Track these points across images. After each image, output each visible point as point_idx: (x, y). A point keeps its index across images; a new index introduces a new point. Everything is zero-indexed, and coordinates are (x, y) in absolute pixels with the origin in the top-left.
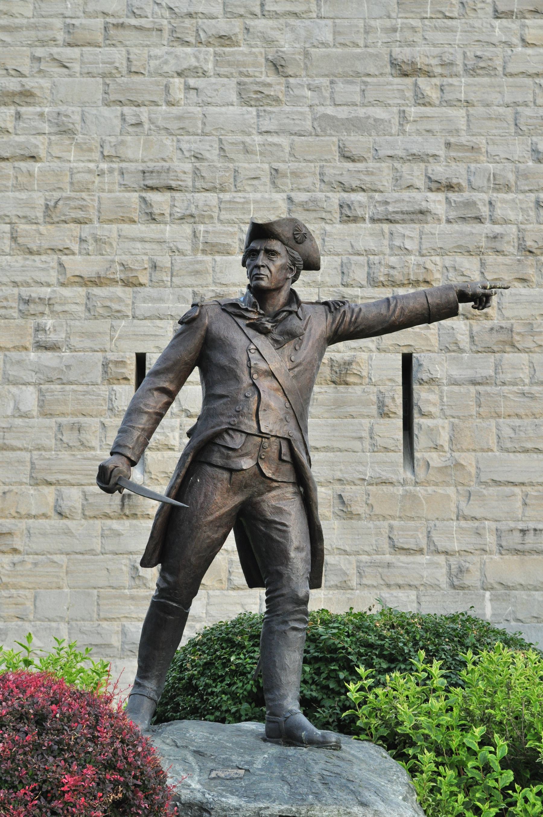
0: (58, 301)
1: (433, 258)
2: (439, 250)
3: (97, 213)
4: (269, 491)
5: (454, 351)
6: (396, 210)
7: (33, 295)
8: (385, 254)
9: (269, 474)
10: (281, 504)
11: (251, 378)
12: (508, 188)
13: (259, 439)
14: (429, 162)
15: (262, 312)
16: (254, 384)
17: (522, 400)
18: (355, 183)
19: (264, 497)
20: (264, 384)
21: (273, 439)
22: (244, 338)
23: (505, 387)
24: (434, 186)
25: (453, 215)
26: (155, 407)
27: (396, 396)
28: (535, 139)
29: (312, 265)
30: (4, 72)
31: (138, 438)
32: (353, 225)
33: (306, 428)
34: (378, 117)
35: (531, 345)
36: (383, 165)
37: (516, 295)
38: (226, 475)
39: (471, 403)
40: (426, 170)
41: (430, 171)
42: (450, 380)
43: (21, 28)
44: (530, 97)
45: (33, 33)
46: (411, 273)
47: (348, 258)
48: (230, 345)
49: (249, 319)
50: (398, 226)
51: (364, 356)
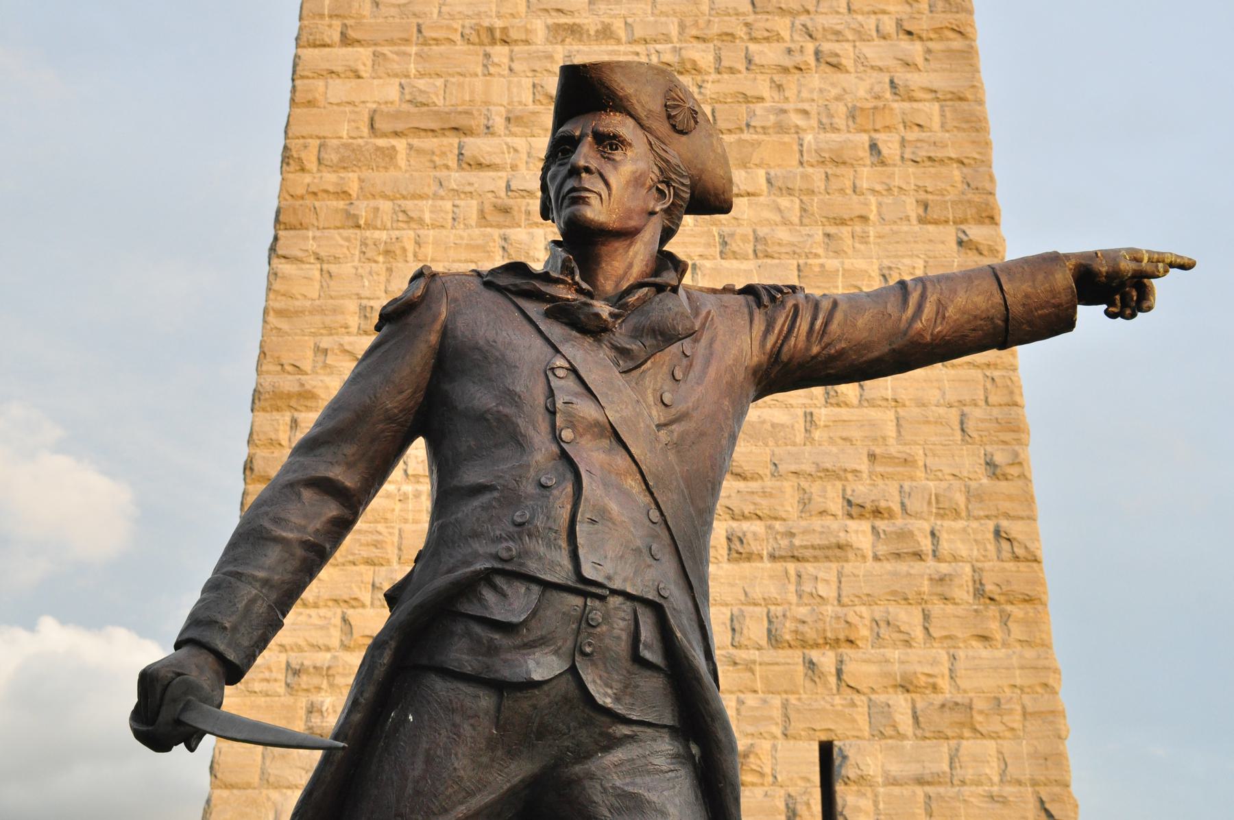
0: (341, 670)
1: (857, 609)
2: (865, 598)
3: (396, 551)
4: (607, 749)
5: (891, 737)
6: (805, 543)
7: (306, 663)
8: (790, 604)
9: (605, 699)
10: (640, 786)
11: (557, 439)
12: (957, 514)
13: (577, 601)
14: (847, 480)
15: (585, 286)
16: (564, 455)
17: (990, 806)
18: (748, 508)
19: (592, 766)
20: (593, 456)
21: (615, 601)
22: (539, 342)
23: (965, 788)
24: (854, 511)
25: (882, 549)
26: (302, 529)
27: (812, 802)
28: (989, 448)
29: (709, 200)
30: (279, 368)
31: (253, 601)
32: (746, 565)
33: (704, 580)
34: (776, 421)
35: (999, 728)
36: (786, 484)
37: (974, 658)
38: (485, 701)
39: (917, 811)
40: (844, 490)
41: (849, 492)
42: (887, 778)
43: (303, 312)
44: (981, 395)
45: (317, 319)
46: (828, 628)
47: (741, 611)
48: (501, 360)
49: (553, 299)
50: (807, 565)
51: (766, 745)
